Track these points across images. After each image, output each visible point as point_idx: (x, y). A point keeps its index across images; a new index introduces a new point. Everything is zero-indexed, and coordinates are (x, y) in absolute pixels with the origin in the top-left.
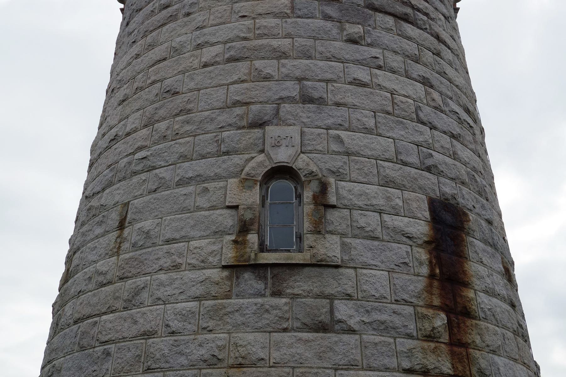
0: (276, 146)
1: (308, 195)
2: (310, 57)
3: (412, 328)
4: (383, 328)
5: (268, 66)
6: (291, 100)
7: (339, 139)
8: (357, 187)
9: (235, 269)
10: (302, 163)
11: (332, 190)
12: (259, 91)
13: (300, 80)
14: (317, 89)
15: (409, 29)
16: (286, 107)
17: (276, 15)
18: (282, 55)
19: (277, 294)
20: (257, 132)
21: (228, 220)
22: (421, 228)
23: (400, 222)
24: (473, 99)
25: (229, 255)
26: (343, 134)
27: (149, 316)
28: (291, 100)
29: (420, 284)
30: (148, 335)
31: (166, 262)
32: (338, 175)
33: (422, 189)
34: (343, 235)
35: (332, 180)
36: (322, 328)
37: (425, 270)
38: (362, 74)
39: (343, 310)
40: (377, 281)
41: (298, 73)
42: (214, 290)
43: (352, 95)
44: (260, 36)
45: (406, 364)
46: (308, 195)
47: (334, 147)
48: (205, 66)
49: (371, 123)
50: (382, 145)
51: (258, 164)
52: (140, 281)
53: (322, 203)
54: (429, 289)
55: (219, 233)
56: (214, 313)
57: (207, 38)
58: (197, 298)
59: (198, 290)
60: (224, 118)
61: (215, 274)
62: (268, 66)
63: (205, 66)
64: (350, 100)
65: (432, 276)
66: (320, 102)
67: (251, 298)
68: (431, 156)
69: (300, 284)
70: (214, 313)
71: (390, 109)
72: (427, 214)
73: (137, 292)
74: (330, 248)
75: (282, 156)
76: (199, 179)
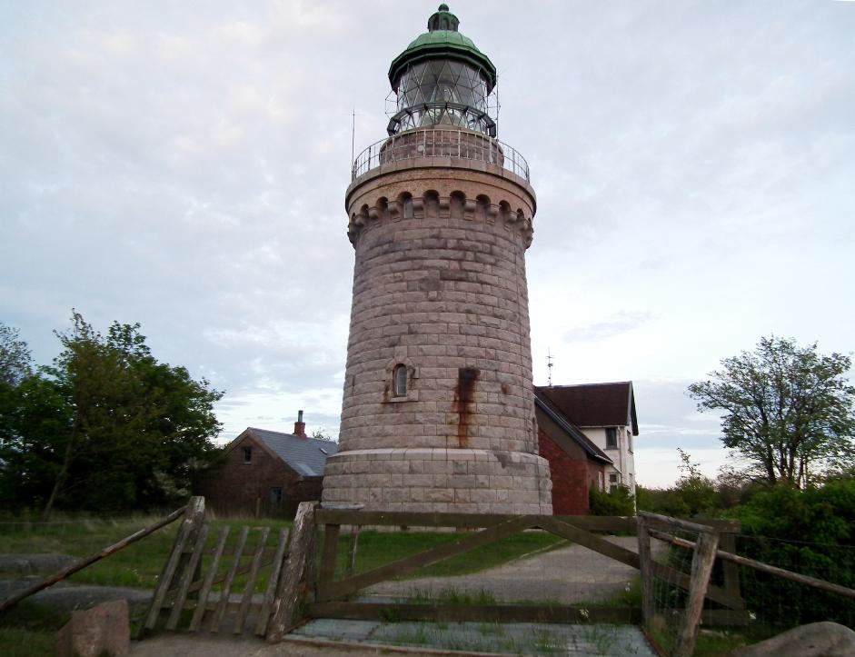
0: (398, 355)
1: (408, 374)
2: (413, 312)
3: (443, 420)
4: (431, 421)
5: (396, 317)
6: (404, 333)
7: (422, 350)
8: (427, 370)
9: (386, 403)
10: (408, 362)
11: (417, 372)
12: (393, 330)
13: (408, 323)
14: (415, 327)
15: (463, 285)
16: (403, 337)
17: (400, 291)
18: (401, 312)
19: (397, 412)
20: (392, 348)
21: (382, 385)
22: (453, 382)
23: (443, 382)
24: (526, 293)
25: (382, 399)
26: (423, 347)
27: (361, 419)
28: (404, 333)
29: (450, 404)
30: (361, 426)
31: (365, 401)
32: (420, 365)
33: (456, 366)
34: (420, 389)
35: (417, 368)
36: (410, 423)
37: (453, 399)
38: (434, 317)
39: (419, 417)
40: (432, 405)
41: (408, 321)
42: (379, 411)
43: (426, 327)
44: (394, 303)
45: (439, 433)
46: (408, 374)
47: (420, 353)
48: (376, 317)
49: (436, 340)
50: (442, 349)
51: (392, 363)
52: (360, 406)
53: (412, 377)
54: (453, 406)
55: (380, 390)
56: (379, 419)
57: (376, 303)
58: (373, 414)
59: (374, 411)
60: (382, 343)
61: (378, 405)
62: (396, 317)
63: (376, 317)
64: (428, 331)
65: (455, 401)
66: (416, 333)
67: (390, 415)
68: (463, 349)
69: (405, 408)
70: (379, 419)
71: (446, 331)
72: (457, 376)
73: (358, 411)
74: (414, 395)
75: (400, 359)
76: (374, 369)
